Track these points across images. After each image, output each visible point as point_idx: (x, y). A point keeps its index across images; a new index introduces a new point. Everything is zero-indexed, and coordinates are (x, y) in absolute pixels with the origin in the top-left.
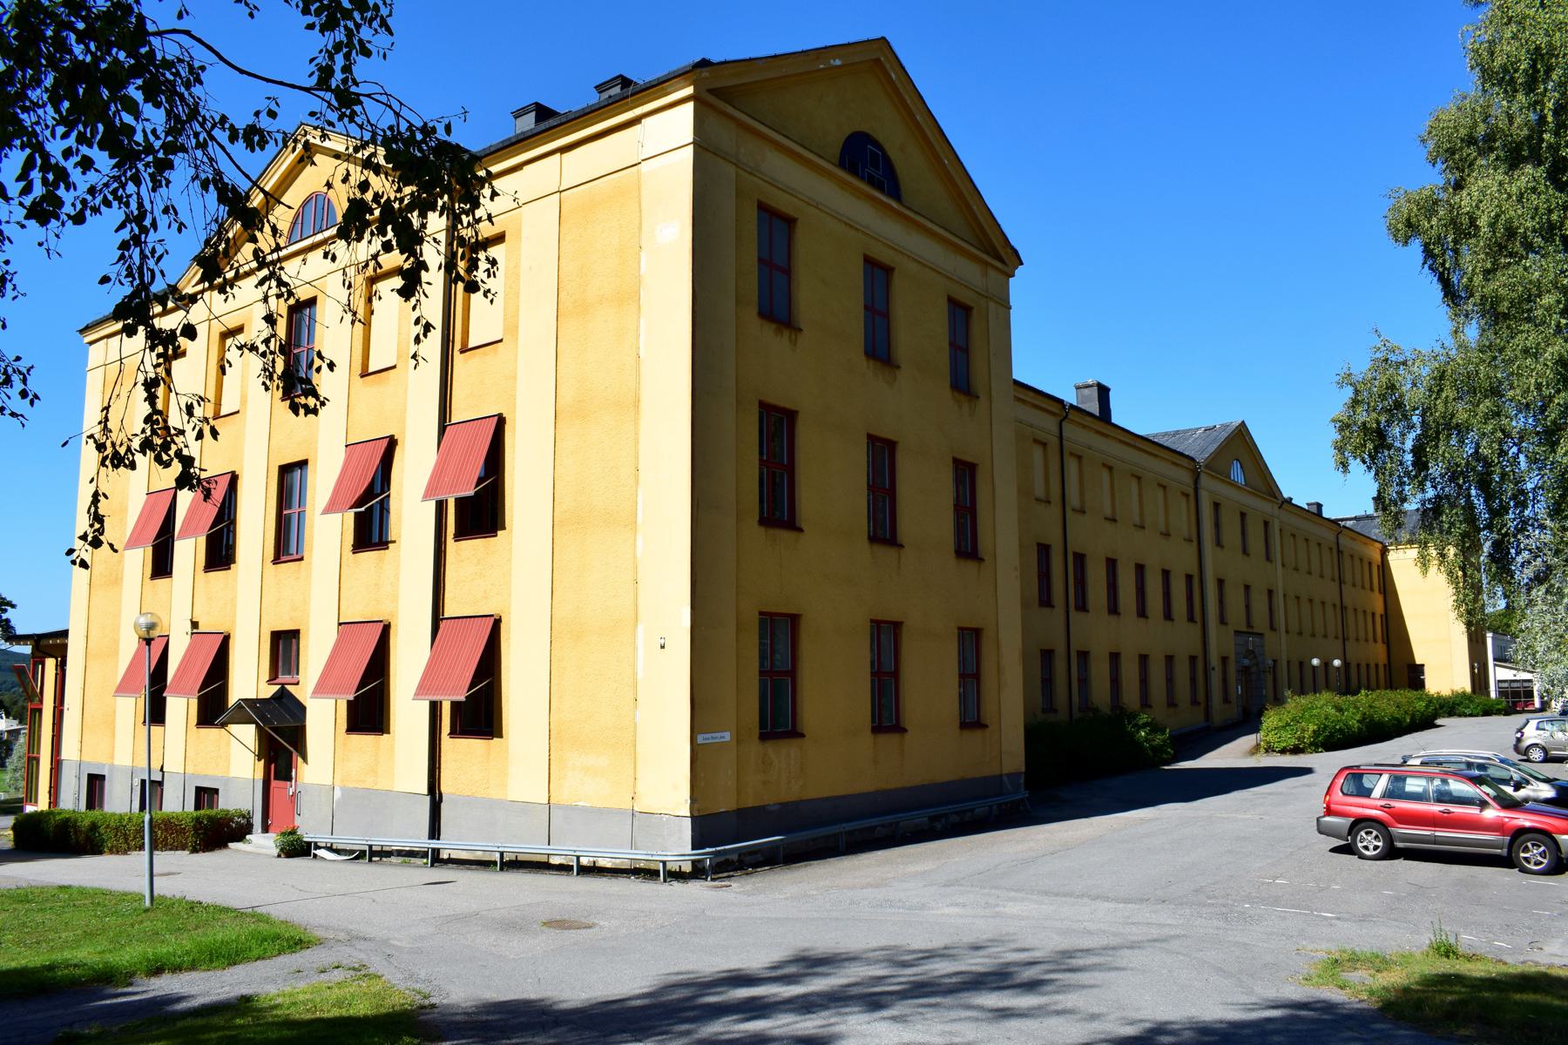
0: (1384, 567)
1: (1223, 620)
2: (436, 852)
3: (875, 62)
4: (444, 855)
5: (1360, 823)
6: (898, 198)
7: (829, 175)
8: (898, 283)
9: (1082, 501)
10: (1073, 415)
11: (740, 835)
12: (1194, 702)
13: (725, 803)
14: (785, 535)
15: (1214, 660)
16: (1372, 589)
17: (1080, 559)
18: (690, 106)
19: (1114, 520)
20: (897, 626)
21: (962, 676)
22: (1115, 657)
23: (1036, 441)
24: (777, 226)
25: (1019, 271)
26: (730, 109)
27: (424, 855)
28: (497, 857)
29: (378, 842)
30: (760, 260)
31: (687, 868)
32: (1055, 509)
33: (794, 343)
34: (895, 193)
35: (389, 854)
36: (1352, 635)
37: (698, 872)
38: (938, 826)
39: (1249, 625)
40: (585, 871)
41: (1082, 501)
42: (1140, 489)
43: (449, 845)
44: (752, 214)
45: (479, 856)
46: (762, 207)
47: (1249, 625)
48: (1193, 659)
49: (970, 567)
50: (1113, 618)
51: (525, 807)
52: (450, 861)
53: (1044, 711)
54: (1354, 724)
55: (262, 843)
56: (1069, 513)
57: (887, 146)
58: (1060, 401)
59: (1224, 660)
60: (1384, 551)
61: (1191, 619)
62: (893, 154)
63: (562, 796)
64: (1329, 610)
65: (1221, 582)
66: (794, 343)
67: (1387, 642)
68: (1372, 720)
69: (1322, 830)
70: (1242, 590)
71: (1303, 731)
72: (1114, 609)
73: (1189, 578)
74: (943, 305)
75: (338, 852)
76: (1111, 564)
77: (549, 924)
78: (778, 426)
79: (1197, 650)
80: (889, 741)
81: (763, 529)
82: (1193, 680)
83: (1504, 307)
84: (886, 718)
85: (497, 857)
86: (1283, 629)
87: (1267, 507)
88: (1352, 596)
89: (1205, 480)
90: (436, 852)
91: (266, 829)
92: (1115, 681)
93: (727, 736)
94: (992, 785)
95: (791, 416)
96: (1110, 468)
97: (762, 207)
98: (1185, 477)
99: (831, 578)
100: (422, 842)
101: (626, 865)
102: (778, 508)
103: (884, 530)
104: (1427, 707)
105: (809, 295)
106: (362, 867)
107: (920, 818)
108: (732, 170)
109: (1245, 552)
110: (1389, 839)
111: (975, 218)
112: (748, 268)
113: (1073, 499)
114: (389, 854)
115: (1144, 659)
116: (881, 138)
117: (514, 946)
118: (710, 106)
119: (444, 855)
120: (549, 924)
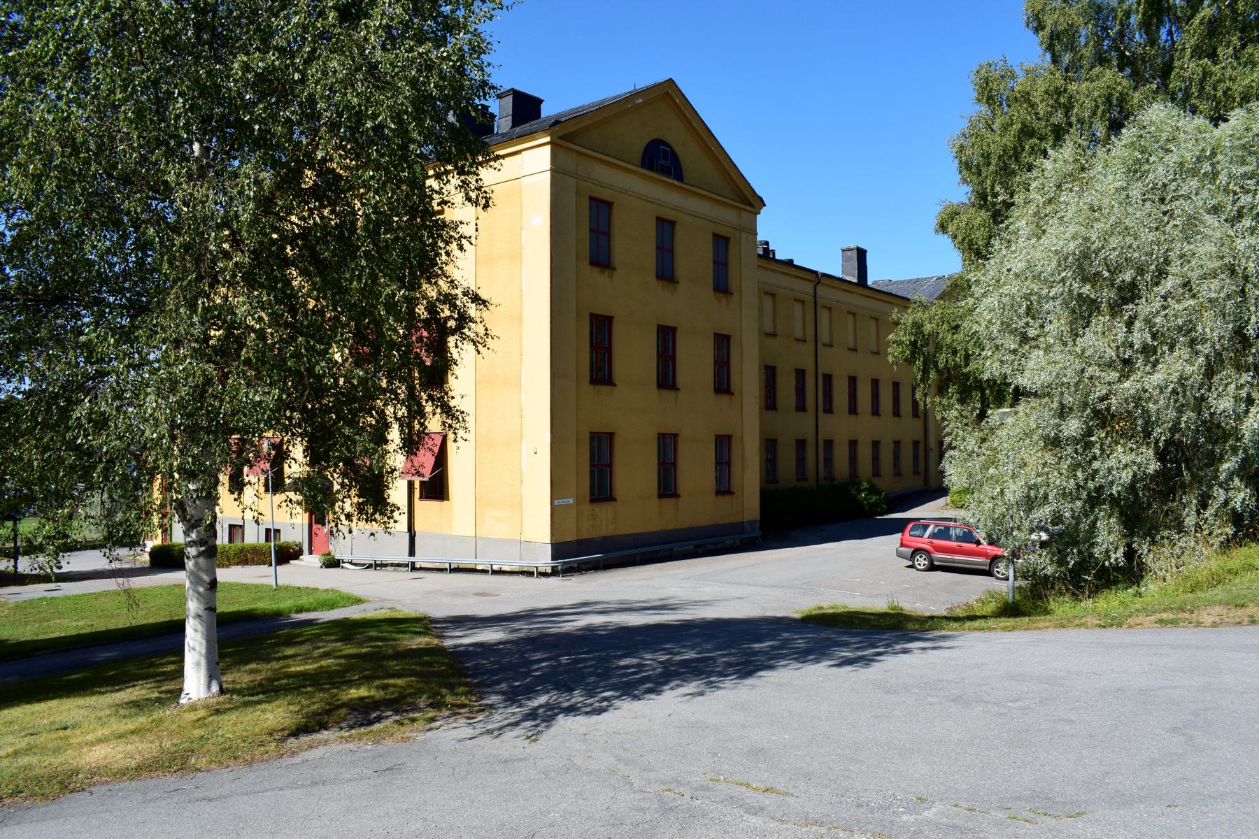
2: (413, 563)
3: (666, 96)
4: (418, 566)
5: (917, 551)
6: (681, 179)
7: (634, 172)
8: (679, 230)
9: (831, 338)
10: (824, 281)
11: (575, 553)
12: (916, 472)
13: (570, 537)
14: (605, 389)
17: (828, 378)
18: (549, 147)
21: (718, 463)
22: (853, 444)
23: (796, 300)
24: (601, 209)
25: (763, 210)
26: (572, 146)
27: (407, 565)
28: (447, 566)
29: (381, 558)
30: (591, 230)
31: (549, 570)
32: (810, 346)
33: (611, 277)
34: (680, 177)
35: (386, 565)
37: (555, 572)
38: (700, 551)
40: (495, 572)
41: (831, 338)
43: (420, 560)
44: (585, 203)
45: (437, 565)
46: (591, 198)
48: (916, 443)
49: (725, 399)
50: (853, 417)
51: (462, 539)
52: (421, 569)
53: (798, 480)
55: (310, 561)
56: (820, 347)
57: (674, 145)
58: (816, 272)
62: (678, 149)
63: (483, 533)
66: (611, 277)
69: (899, 555)
72: (853, 410)
74: (710, 238)
75: (355, 564)
76: (853, 381)
77: (477, 594)
78: (601, 327)
79: (919, 436)
80: (669, 503)
81: (591, 387)
82: (916, 458)
84: (667, 488)
85: (447, 566)
90: (413, 563)
91: (311, 552)
92: (853, 459)
93: (571, 501)
94: (738, 527)
95: (610, 319)
96: (854, 314)
97: (591, 198)
99: (634, 411)
100: (405, 558)
101: (517, 569)
102: (602, 374)
103: (667, 380)
105: (620, 248)
106: (371, 572)
107: (690, 547)
108: (573, 181)
110: (931, 561)
111: (732, 179)
112: (585, 235)
113: (824, 336)
114: (386, 565)
115: (876, 444)
116: (669, 140)
117: (460, 601)
118: (561, 146)
119: (418, 566)
120: (477, 594)
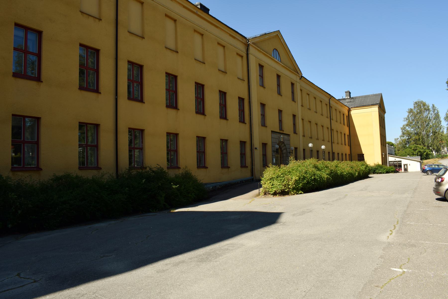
0: (349, 117)
1: (264, 124)
12: (243, 165)
15: (257, 143)
16: (344, 124)
19: (225, 72)
20: (176, 135)
36: (336, 141)
39: (281, 128)
42: (309, 98)
47: (281, 128)
48: (243, 144)
54: (325, 175)
59: (264, 145)
60: (349, 111)
61: (242, 120)
64: (325, 130)
65: (263, 106)
67: (350, 146)
68: (336, 174)
70: (291, 117)
71: (288, 180)
73: (241, 100)
83: (419, 111)
86: (301, 134)
87: (295, 78)
88: (335, 126)
89: (252, 50)
98: (241, 48)
104: (365, 168)
109: (279, 93)
